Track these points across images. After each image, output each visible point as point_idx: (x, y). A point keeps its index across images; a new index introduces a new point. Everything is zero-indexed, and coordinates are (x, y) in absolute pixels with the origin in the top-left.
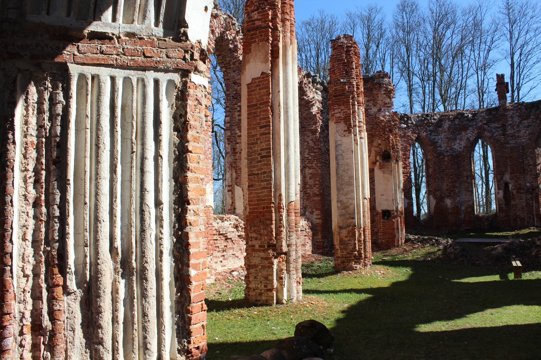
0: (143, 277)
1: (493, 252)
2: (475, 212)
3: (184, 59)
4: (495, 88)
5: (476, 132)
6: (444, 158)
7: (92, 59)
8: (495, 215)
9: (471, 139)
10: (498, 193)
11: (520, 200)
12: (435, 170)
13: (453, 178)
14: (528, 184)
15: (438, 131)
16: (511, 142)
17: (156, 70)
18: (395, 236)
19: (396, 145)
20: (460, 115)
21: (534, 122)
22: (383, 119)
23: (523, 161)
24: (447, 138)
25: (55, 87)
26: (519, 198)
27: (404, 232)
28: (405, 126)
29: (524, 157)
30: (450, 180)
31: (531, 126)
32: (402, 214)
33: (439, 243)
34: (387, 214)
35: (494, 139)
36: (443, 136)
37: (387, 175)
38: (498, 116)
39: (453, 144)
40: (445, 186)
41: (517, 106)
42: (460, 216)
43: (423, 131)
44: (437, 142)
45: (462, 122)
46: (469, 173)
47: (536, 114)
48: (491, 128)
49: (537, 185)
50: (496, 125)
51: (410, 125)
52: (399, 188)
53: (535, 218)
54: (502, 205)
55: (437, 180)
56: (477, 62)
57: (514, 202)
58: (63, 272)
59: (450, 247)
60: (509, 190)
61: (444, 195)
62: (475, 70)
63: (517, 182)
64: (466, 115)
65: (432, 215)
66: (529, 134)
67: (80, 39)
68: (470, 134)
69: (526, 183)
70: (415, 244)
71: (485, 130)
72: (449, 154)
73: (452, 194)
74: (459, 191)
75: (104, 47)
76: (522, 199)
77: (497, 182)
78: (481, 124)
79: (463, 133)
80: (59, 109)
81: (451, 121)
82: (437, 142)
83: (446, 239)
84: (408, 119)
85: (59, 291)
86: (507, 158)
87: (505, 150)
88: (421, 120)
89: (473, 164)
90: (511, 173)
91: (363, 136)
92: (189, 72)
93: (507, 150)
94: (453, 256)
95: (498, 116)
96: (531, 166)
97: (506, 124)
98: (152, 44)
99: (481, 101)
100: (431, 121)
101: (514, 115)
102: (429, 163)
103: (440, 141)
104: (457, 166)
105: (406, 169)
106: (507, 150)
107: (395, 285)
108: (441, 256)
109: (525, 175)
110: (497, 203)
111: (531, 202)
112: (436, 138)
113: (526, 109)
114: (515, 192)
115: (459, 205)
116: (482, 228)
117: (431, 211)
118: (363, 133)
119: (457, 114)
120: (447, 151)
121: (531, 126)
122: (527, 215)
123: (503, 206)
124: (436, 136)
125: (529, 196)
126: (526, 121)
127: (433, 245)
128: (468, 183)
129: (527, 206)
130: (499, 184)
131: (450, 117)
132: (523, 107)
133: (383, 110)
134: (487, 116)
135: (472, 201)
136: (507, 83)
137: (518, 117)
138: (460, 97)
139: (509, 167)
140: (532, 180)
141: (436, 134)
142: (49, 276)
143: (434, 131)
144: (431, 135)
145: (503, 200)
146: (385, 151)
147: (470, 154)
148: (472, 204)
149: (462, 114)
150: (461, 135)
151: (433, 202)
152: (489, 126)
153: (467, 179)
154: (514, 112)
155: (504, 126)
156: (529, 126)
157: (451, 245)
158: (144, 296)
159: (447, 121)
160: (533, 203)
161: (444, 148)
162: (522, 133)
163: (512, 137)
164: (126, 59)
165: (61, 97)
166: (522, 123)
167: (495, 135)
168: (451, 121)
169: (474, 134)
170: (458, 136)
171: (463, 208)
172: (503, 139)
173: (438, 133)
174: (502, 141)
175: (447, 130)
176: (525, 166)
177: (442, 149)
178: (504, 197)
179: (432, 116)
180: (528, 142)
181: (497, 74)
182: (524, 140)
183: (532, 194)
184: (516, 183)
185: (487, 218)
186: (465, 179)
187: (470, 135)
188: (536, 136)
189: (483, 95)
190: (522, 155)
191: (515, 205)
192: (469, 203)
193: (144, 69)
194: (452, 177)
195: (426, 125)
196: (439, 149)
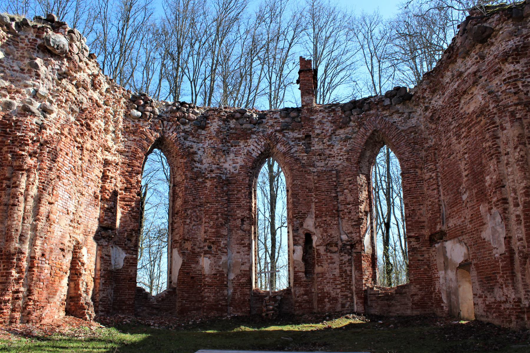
2: (254, 285)
5: (263, 143)
6: (204, 182)
9: (255, 154)
10: (294, 251)
11: (331, 265)
12: (185, 202)
13: (217, 219)
14: (344, 237)
15: (199, 135)
16: (318, 164)
21: (354, 133)
23: (337, 196)
26: (329, 261)
28: (140, 114)
29: (338, 190)
30: (212, 223)
31: (350, 138)
35: (291, 157)
36: (207, 145)
38: (299, 120)
39: (222, 160)
40: (203, 233)
42: (226, 292)
43: (171, 130)
44: (195, 153)
45: (242, 125)
46: (246, 213)
47: (359, 118)
49: (358, 238)
50: (296, 135)
51: (148, 113)
53: (355, 298)
54: (300, 274)
55: (188, 221)
57: (320, 268)
60: (311, 247)
61: (199, 250)
63: (326, 232)
65: (175, 286)
66: (348, 152)
69: (340, 234)
72: (214, 175)
73: (214, 248)
74: (226, 245)
76: (335, 263)
77: (293, 230)
78: (271, 130)
82: (195, 153)
84: (146, 103)
87: (309, 177)
88: (172, 111)
89: (255, 199)
93: (311, 177)
95: (299, 120)
96: (349, 204)
97: (311, 133)
100: (189, 116)
101: (325, 120)
104: (226, 198)
105: (130, 192)
106: (311, 177)
109: (340, 221)
110: (291, 269)
111: (349, 268)
112: (195, 145)
113: (344, 112)
114: (322, 249)
115: (225, 270)
116: (264, 314)
117: (173, 278)
120: (212, 171)
121: (350, 138)
122: (341, 291)
123: (302, 275)
124: (195, 142)
125: (346, 258)
126: (342, 131)
128: (244, 231)
129: (341, 276)
130: (295, 234)
131: (222, 114)
132: (339, 109)
134: (283, 118)
135: (248, 264)
137: (331, 122)
140: (351, 229)
144: (185, 139)
145: (302, 264)
147: (251, 181)
148: (248, 269)
150: (238, 147)
152: (284, 136)
153: (243, 224)
154: (324, 115)
155: (308, 136)
156: (346, 139)
159: (216, 120)
160: (351, 271)
161: (206, 166)
162: (335, 150)
163: (320, 155)
166: (337, 133)
167: (293, 151)
168: (224, 121)
169: (258, 147)
170: (232, 148)
171: (232, 276)
172: (305, 158)
173: (198, 137)
174: (303, 162)
175: (214, 134)
176: (339, 205)
178: (304, 259)
179: (190, 107)
180: (345, 164)
181: (301, 57)
182: (338, 162)
183: (350, 254)
184: (325, 234)
186: (239, 222)
187: (252, 147)
188: (358, 154)
190: (336, 186)
191: (322, 273)
192: (243, 268)
194: (215, 216)
195: (178, 120)
196: (198, 165)
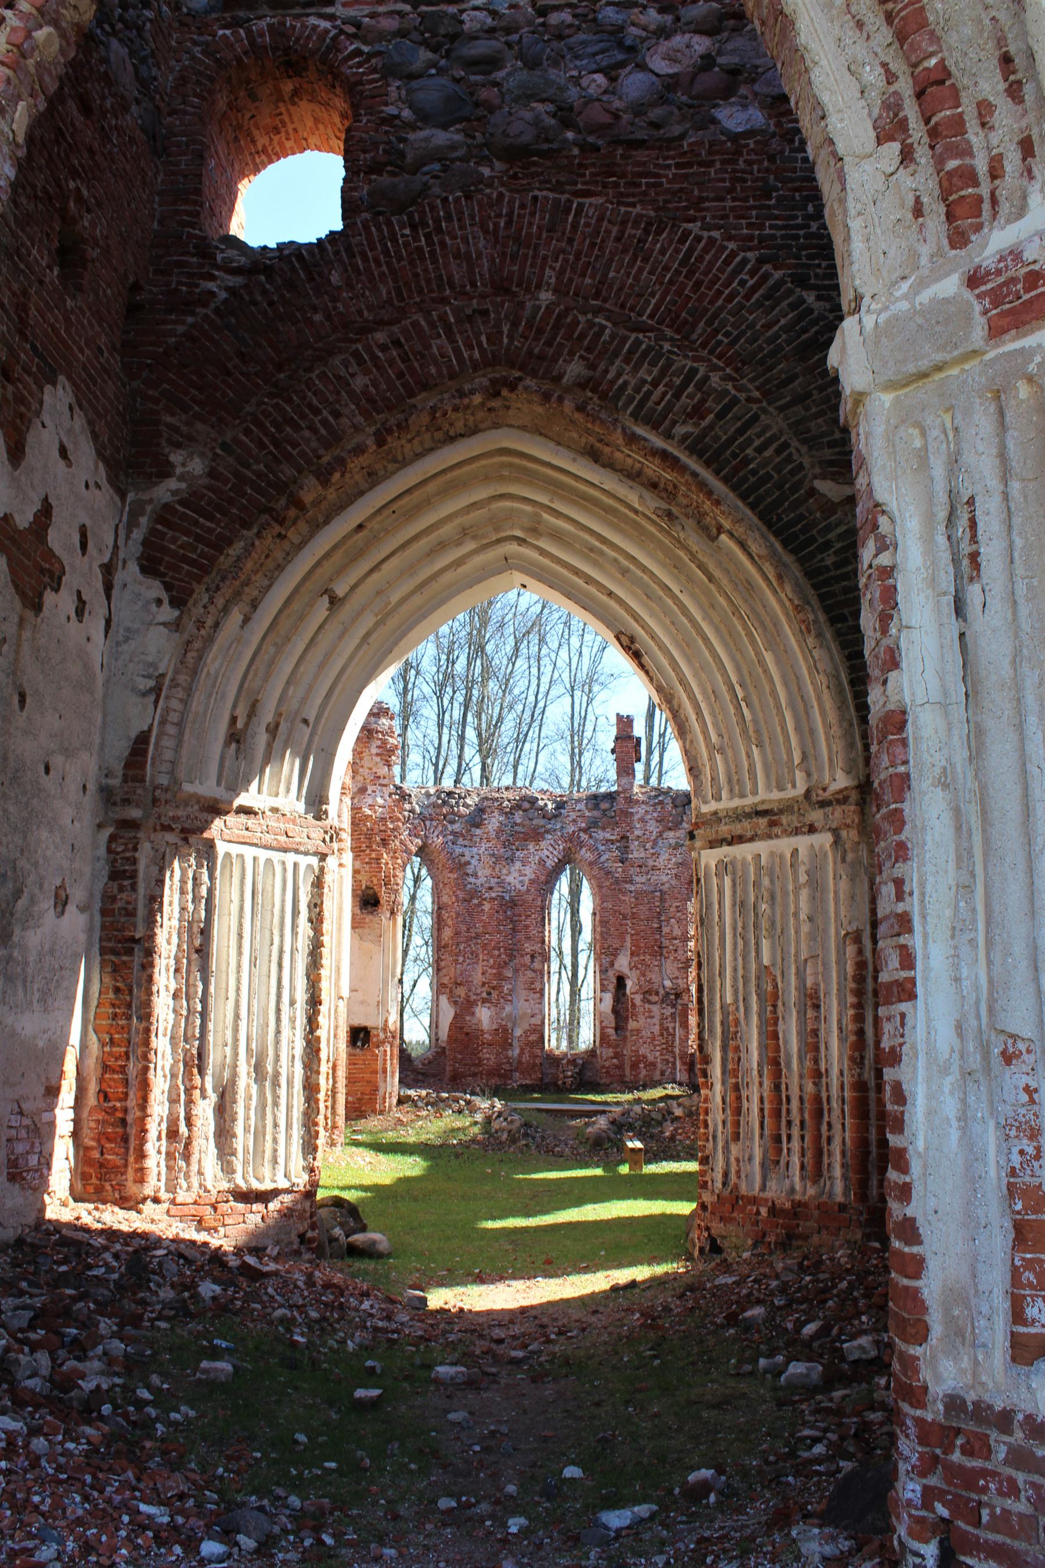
0: (276, 1084)
1: (589, 1130)
3: (324, 841)
4: (612, 745)
6: (480, 904)
7: (238, 836)
8: (592, 1053)
12: (457, 933)
14: (668, 983)
16: (638, 879)
17: (297, 851)
18: (376, 1089)
19: (395, 876)
20: (528, 803)
22: (369, 812)
24: (493, 855)
25: (199, 866)
27: (397, 1079)
30: (492, 961)
32: (394, 1037)
33: (473, 1109)
34: (362, 1035)
35: (600, 869)
37: (368, 945)
39: (504, 871)
41: (656, 796)
42: (510, 1053)
44: (468, 863)
46: (537, 947)
48: (596, 840)
50: (608, 836)
52: (393, 976)
55: (461, 959)
56: (574, 667)
58: (201, 1072)
59: (499, 1116)
60: (624, 994)
62: (568, 686)
64: (541, 803)
67: (227, 813)
68: (548, 850)
70: (419, 1109)
71: (581, 845)
72: (493, 895)
73: (495, 994)
74: (511, 990)
75: (250, 825)
79: (531, 847)
80: (204, 891)
81: (506, 813)
82: (468, 863)
83: (490, 1098)
85: (197, 1093)
86: (625, 918)
88: (434, 805)
90: (632, 954)
91: (343, 861)
92: (326, 855)
94: (505, 1136)
98: (294, 823)
99: (576, 766)
102: (445, 915)
103: (474, 862)
107: (404, 1181)
108: (480, 1137)
112: (467, 851)
114: (638, 999)
115: (510, 1025)
117: (440, 1034)
118: (344, 855)
119: (521, 799)
120: (491, 888)
123: (611, 1031)
125: (668, 1011)
126: (671, 834)
127: (460, 1112)
128: (534, 971)
129: (662, 1035)
132: (668, 800)
133: (369, 792)
134: (590, 810)
136: (639, 740)
138: (527, 746)
139: (628, 938)
140: (677, 973)
141: (466, 843)
142: (188, 1075)
143: (463, 835)
145: (612, 1017)
146: (367, 887)
147: (543, 901)
149: (533, 801)
151: (448, 1013)
152: (591, 837)
153: (532, 961)
157: (500, 1114)
158: (276, 1104)
161: (482, 880)
164: (268, 838)
165: (205, 877)
167: (603, 859)
168: (506, 813)
171: (518, 1032)
175: (493, 835)
177: (479, 882)
178: (615, 1011)
179: (460, 797)
182: (665, 879)
183: (674, 1006)
185: (573, 1062)
186: (528, 958)
187: (546, 852)
189: (581, 754)
192: (533, 1021)
193: (285, 850)
194: (496, 952)
196: (472, 880)
